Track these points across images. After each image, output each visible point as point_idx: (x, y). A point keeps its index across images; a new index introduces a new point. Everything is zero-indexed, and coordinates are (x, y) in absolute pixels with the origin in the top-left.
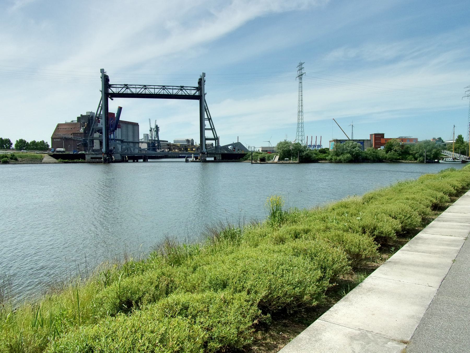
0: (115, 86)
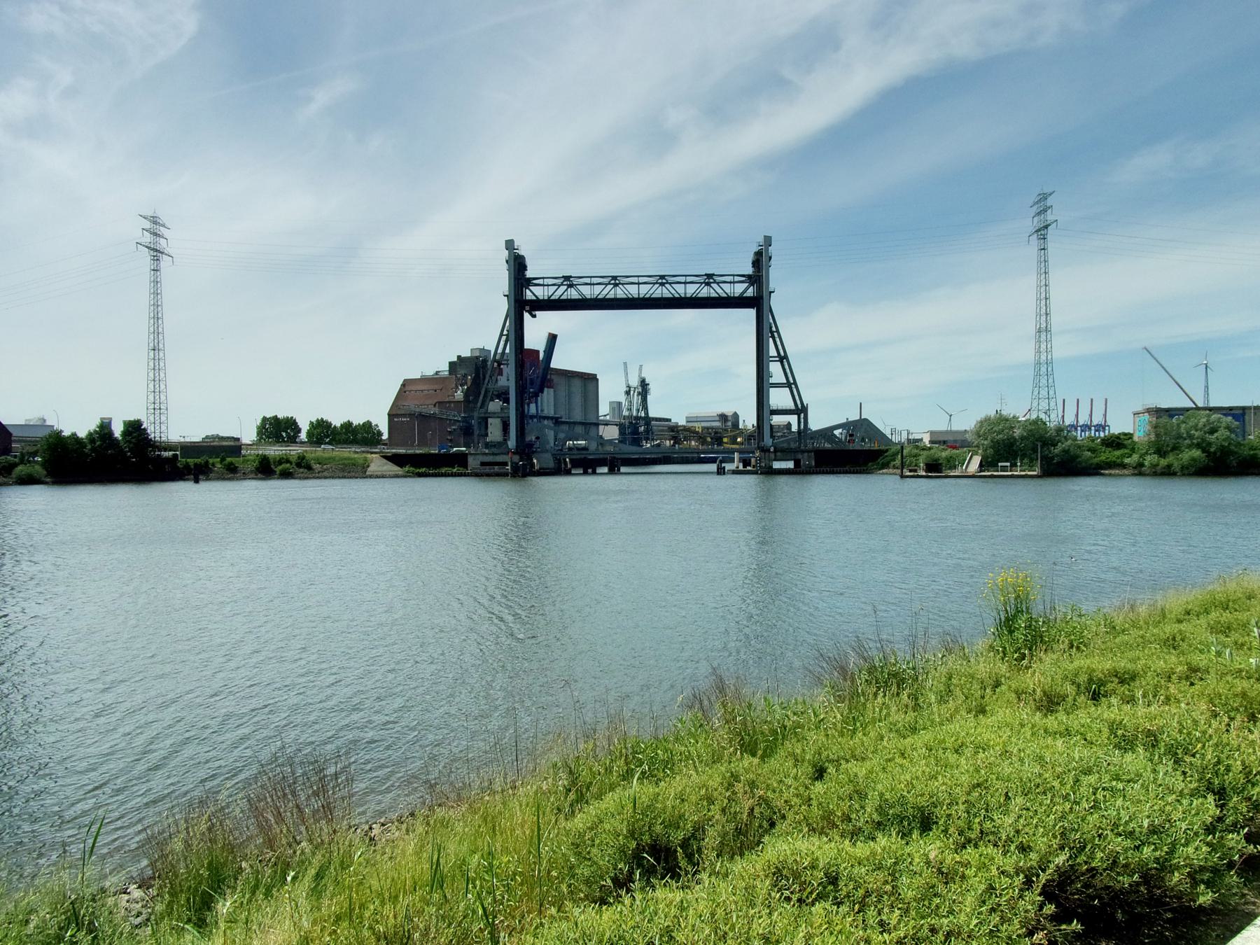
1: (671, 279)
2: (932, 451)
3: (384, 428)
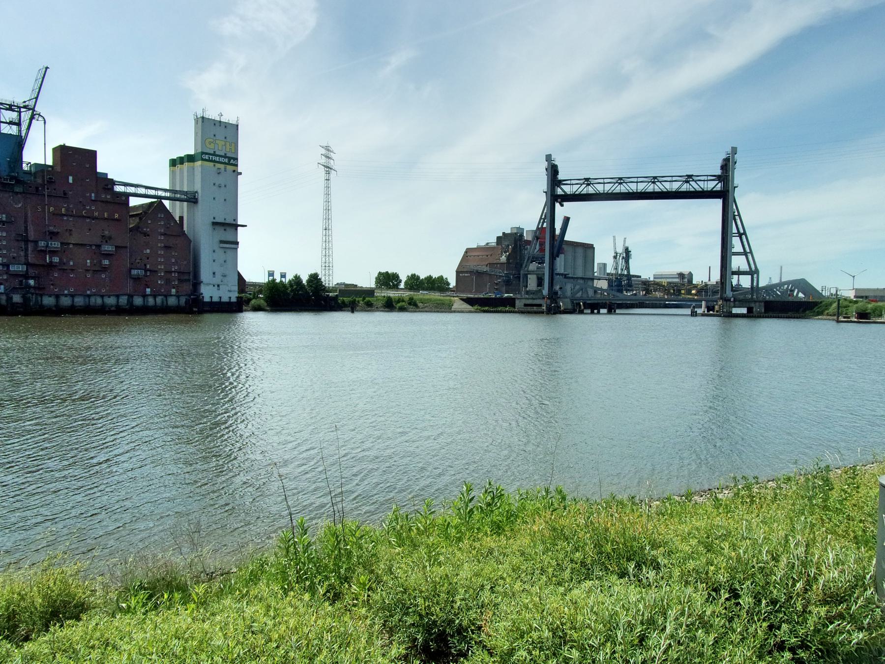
0: (568, 182)
1: (661, 179)
2: (860, 304)
3: (453, 283)
